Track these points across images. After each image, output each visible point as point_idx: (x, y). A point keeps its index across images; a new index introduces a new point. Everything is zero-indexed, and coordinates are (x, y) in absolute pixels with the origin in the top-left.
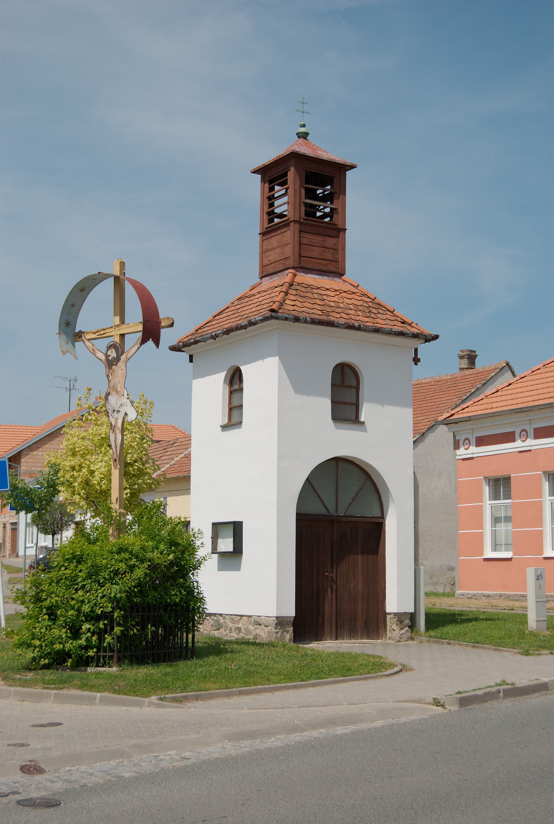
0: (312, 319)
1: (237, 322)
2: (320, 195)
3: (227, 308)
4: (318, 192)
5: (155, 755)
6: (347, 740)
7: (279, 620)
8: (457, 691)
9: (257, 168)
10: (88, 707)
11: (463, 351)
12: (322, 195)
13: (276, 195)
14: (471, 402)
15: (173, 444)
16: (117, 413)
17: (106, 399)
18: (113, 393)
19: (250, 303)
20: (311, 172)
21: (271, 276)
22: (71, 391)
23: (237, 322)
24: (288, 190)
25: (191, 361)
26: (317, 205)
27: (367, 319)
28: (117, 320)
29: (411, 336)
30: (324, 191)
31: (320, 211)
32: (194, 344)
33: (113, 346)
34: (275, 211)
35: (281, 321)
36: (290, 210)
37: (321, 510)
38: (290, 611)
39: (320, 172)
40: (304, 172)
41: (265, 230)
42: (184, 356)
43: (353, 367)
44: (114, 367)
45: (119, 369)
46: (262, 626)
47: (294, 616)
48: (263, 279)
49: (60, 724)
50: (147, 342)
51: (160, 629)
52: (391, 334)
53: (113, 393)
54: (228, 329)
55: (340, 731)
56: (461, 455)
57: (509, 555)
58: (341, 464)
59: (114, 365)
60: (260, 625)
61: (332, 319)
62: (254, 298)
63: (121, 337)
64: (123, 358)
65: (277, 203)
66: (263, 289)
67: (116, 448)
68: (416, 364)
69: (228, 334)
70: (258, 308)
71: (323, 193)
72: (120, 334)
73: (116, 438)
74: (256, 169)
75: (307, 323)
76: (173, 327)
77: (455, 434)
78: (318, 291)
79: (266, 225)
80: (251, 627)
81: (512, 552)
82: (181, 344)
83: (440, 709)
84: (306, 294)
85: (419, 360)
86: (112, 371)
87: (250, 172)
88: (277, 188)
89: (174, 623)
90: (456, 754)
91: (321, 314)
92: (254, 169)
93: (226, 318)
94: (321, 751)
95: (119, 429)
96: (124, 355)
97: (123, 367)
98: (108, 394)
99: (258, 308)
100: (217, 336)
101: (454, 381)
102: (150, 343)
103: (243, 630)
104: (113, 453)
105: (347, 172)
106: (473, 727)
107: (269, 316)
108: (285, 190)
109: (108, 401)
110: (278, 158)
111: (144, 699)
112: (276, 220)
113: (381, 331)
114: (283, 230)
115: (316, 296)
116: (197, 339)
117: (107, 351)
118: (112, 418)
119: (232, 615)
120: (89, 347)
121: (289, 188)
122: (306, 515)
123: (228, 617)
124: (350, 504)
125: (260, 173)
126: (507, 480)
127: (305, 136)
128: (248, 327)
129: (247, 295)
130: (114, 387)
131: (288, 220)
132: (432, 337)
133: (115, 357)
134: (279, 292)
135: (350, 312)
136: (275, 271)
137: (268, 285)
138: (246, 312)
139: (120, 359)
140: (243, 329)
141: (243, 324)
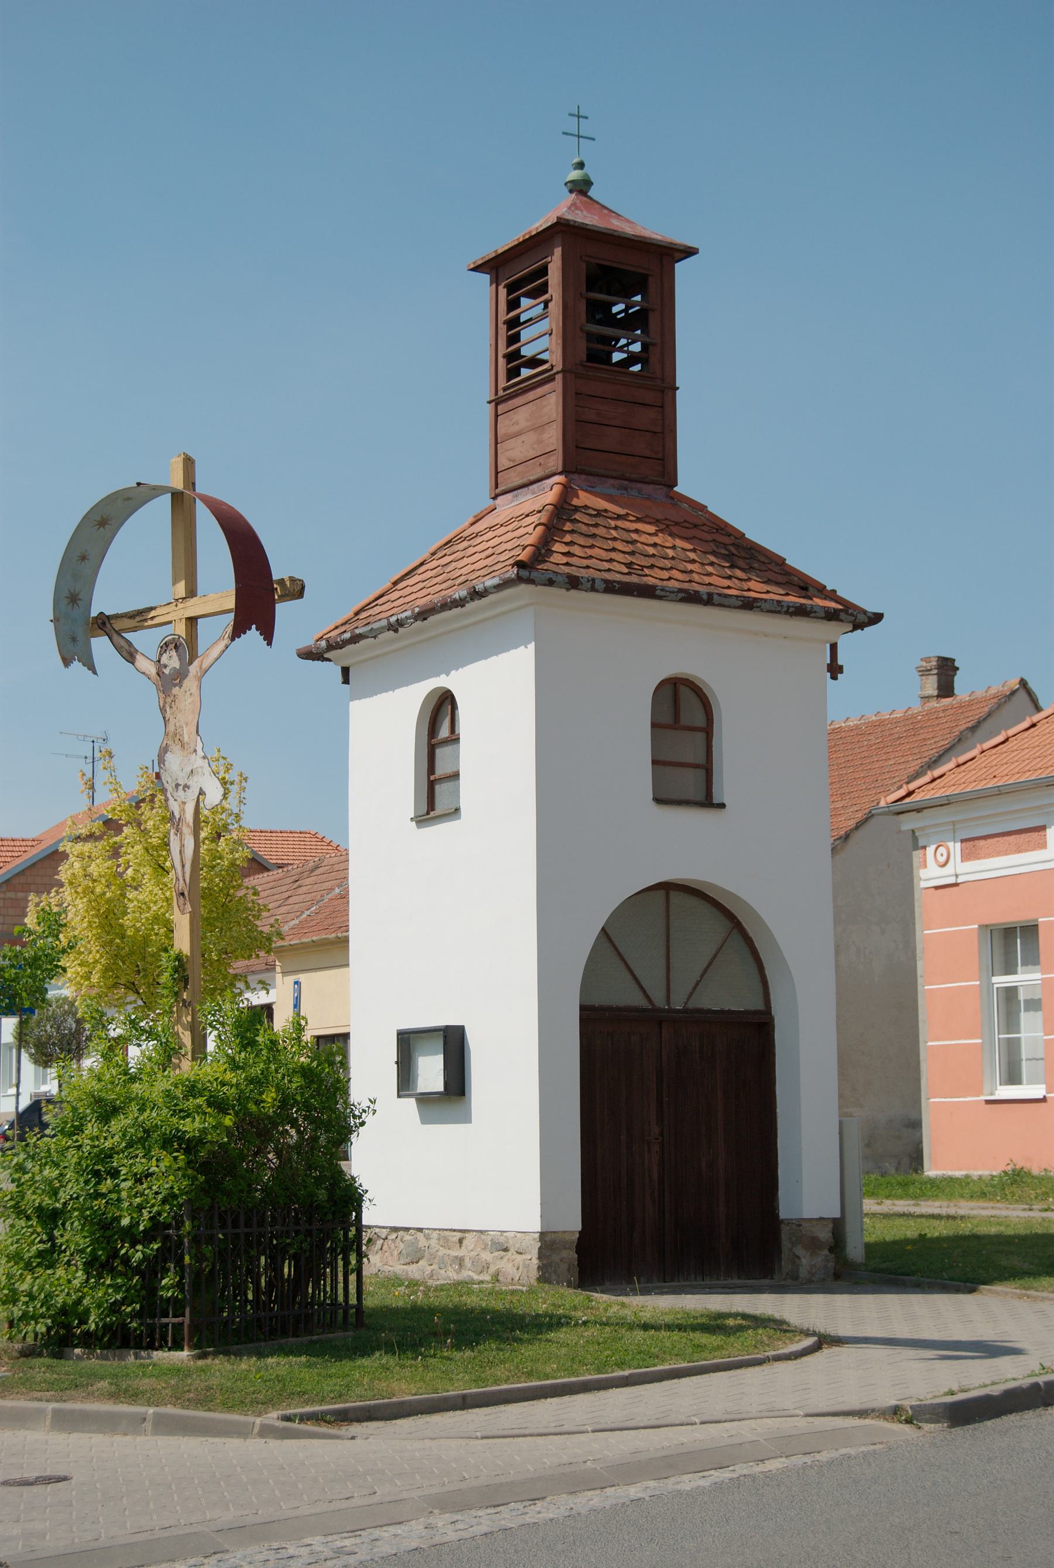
0: (606, 581)
1: (443, 593)
2: (619, 317)
3: (422, 564)
4: (615, 309)
5: (275, 1545)
6: (705, 1503)
7: (547, 1239)
8: (946, 1390)
9: (482, 258)
10: (128, 1438)
11: (927, 660)
12: (623, 315)
13: (523, 319)
14: (951, 765)
15: (312, 871)
16: (184, 789)
17: (161, 760)
18: (176, 748)
19: (472, 550)
20: (598, 265)
21: (515, 493)
22: (95, 763)
23: (443, 593)
24: (550, 304)
25: (346, 680)
26: (612, 338)
27: (727, 583)
28: (181, 589)
29: (824, 615)
30: (628, 308)
31: (621, 349)
32: (351, 644)
33: (170, 645)
34: (522, 353)
35: (539, 587)
36: (554, 348)
37: (636, 1000)
38: (572, 1222)
39: (614, 265)
40: (584, 266)
41: (501, 393)
42: (331, 671)
43: (698, 687)
44: (176, 690)
45: (187, 694)
46: (510, 1253)
47: (580, 1229)
48: (500, 498)
49: (65, 1479)
50: (245, 633)
51: (287, 1261)
52: (779, 612)
53: (176, 748)
54: (424, 609)
55: (688, 1483)
56: (929, 879)
57: (1037, 1091)
58: (676, 898)
59: (175, 685)
60: (506, 1250)
61: (650, 581)
62: (479, 540)
63: (189, 625)
64: (194, 669)
65: (526, 334)
66: (500, 520)
67: (183, 866)
68: (834, 677)
69: (425, 619)
70: (489, 561)
71: (625, 311)
72: (187, 619)
73: (182, 846)
74: (480, 262)
75: (597, 591)
76: (302, 597)
77: (916, 834)
78: (620, 523)
79: (502, 383)
80: (486, 1256)
81: (1044, 1086)
82: (323, 643)
83: (907, 1429)
84: (594, 530)
85: (840, 669)
86: (172, 698)
87: (466, 269)
88: (525, 302)
89: (141, 1228)
90: (951, 1532)
91: (626, 570)
92: (474, 263)
93: (421, 585)
94: (647, 1531)
95: (188, 826)
96: (196, 663)
97: (194, 690)
98: (164, 750)
99: (489, 561)
100: (400, 623)
101: (911, 724)
102: (253, 635)
103: (468, 1263)
104: (177, 879)
105: (676, 265)
106: (984, 1470)
107: (513, 576)
108: (542, 306)
109: (164, 765)
110: (527, 237)
111: (251, 1419)
112: (525, 372)
113: (757, 607)
114: (539, 391)
115: (614, 533)
116: (357, 631)
117: (161, 655)
118: (175, 803)
119: (444, 1230)
120: (122, 647)
121: (551, 300)
122: (602, 1009)
123: (435, 1235)
124: (697, 984)
125: (488, 270)
126: (1030, 930)
127: (584, 188)
128: (468, 602)
129: (464, 534)
130: (176, 735)
131: (552, 369)
132: (868, 617)
133: (178, 667)
134: (534, 525)
135: (690, 567)
136: (525, 480)
137: (511, 510)
138: (464, 571)
139: (189, 672)
140: (456, 607)
141: (457, 596)
